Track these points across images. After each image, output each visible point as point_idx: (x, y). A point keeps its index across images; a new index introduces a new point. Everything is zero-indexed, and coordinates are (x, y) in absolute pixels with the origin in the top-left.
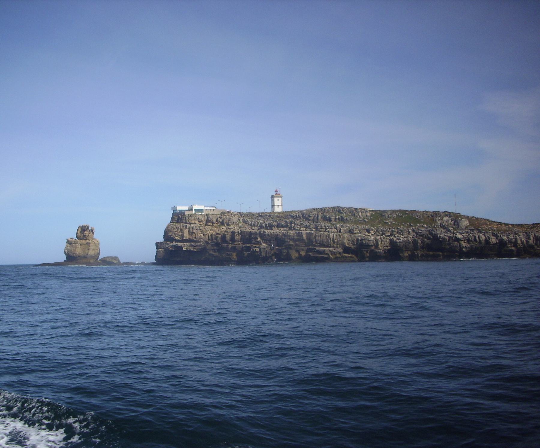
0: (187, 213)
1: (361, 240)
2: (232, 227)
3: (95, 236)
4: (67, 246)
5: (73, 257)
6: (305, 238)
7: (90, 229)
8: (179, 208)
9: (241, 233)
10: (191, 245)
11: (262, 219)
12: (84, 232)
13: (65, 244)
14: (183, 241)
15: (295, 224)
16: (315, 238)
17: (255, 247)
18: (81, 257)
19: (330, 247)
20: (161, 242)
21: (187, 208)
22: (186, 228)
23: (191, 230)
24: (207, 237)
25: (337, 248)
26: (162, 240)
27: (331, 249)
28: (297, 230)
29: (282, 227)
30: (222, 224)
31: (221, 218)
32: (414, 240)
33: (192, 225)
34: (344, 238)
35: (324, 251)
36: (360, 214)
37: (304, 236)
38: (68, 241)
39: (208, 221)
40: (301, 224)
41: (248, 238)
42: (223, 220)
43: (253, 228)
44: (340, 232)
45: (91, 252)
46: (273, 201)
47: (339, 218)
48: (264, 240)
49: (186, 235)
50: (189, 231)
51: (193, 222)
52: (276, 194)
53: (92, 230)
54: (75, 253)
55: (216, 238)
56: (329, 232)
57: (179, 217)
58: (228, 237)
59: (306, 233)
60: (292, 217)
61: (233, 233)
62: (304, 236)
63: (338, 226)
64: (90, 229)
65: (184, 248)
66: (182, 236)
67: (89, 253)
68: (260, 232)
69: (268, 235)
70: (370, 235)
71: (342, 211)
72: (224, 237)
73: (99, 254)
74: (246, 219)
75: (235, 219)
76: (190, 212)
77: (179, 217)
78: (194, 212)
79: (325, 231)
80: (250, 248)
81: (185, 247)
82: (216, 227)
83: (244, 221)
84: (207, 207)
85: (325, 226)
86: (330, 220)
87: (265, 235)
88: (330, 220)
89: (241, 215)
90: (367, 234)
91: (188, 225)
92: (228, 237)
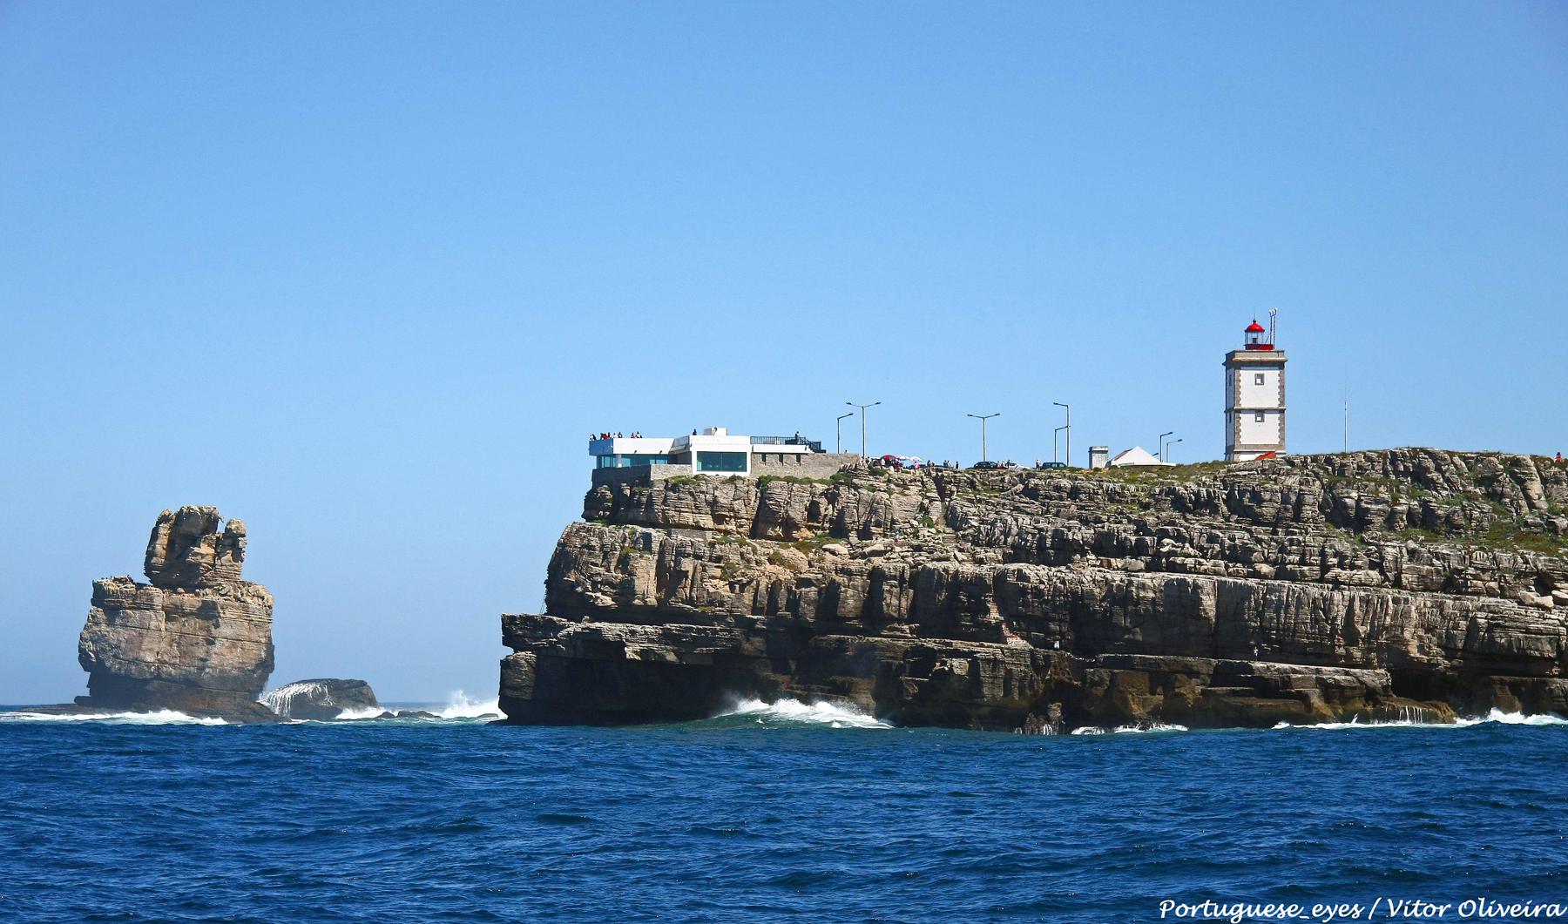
0: (660, 473)
1: (1490, 628)
2: (878, 544)
3: (247, 570)
4: (93, 620)
5: (127, 677)
6: (1212, 614)
7: (221, 528)
8: (622, 446)
9: (920, 580)
10: (667, 637)
11: (1035, 506)
12: (189, 549)
13: (84, 606)
14: (626, 609)
16: (1260, 615)
17: (957, 654)
18: (171, 680)
19: (1332, 660)
20: (527, 619)
21: (665, 446)
22: (647, 547)
23: (670, 559)
24: (748, 597)
25: (1367, 665)
26: (536, 605)
27: (1328, 672)
28: (1183, 568)
29: (1122, 550)
30: (838, 530)
31: (832, 498)
33: (679, 537)
34: (1406, 615)
35: (1286, 681)
36: (1536, 488)
37: (1209, 602)
38: (100, 595)
39: (767, 520)
40: (1212, 539)
41: (946, 605)
42: (841, 513)
43: (982, 553)
44: (1397, 583)
45: (225, 657)
47: (1410, 513)
48: (1020, 617)
49: (646, 583)
50: (661, 568)
51: (689, 518)
53: (231, 543)
54: (137, 661)
55: (793, 604)
56: (1337, 584)
57: (620, 491)
58: (851, 600)
59: (1221, 589)
60: (1179, 503)
61: (877, 576)
62: (1209, 602)
63: (1390, 552)
64: (221, 528)
65: (630, 652)
66: (625, 590)
67: (214, 661)
68: (1000, 578)
69: (1038, 593)
70: (1548, 601)
71: (1435, 475)
72: (830, 594)
74: (959, 502)
75: (902, 506)
76: (676, 470)
77: (620, 491)
78: (694, 468)
79: (1322, 580)
80: (931, 655)
81: (636, 640)
82: (803, 546)
84: (772, 441)
85: (1323, 554)
86: (1357, 522)
87: (1023, 591)
88: (1357, 522)
89: (941, 480)
90: (1533, 596)
91: (657, 535)
92: (851, 600)
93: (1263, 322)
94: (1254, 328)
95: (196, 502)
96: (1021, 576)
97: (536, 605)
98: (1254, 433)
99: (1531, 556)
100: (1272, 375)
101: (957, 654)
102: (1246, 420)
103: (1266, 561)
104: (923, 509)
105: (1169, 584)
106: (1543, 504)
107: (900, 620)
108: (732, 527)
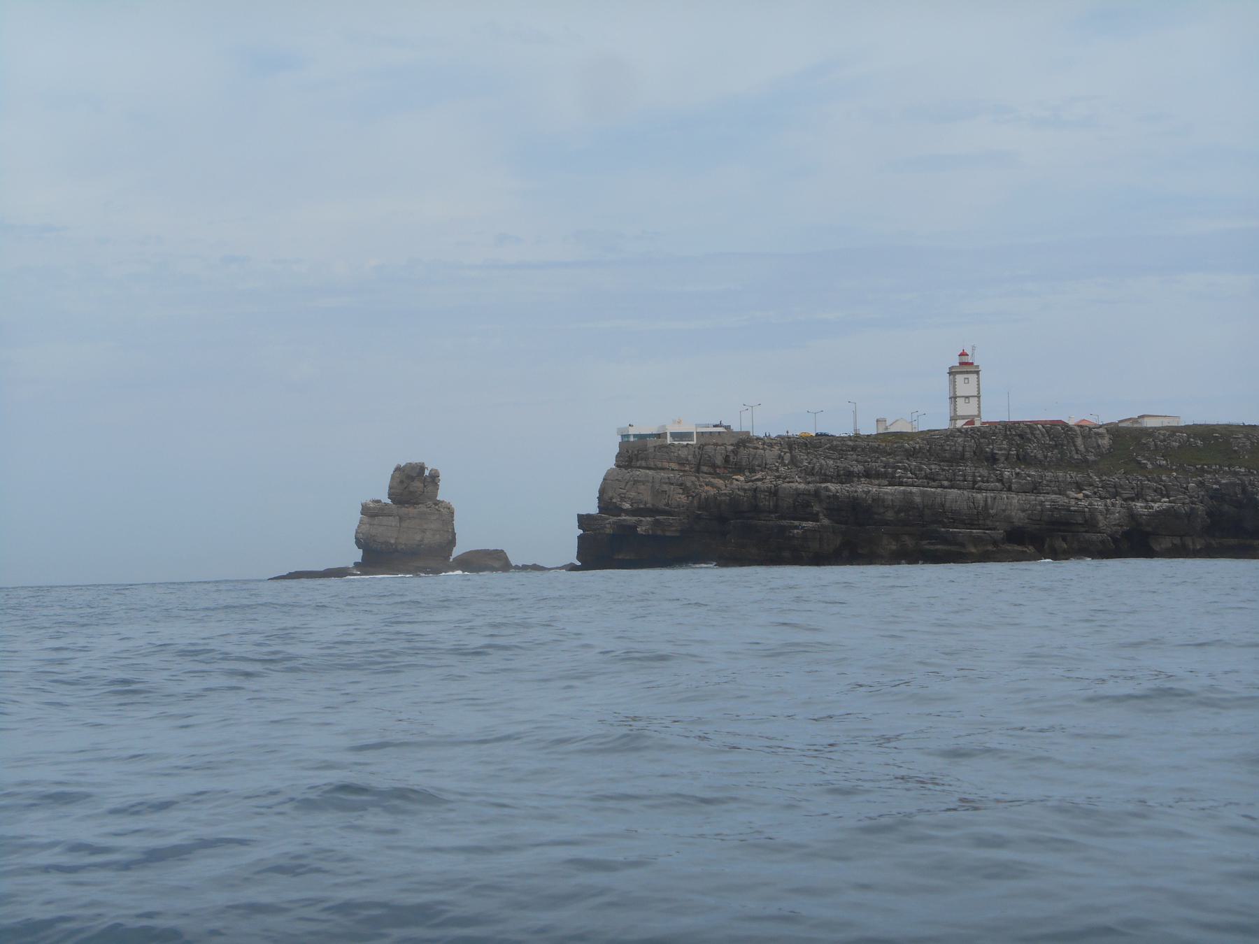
7: (427, 473)
12: (414, 486)
13: (357, 516)
15: (905, 469)
17: (796, 527)
20: (588, 516)
26: (593, 509)
29: (878, 475)
30: (740, 470)
32: (1192, 509)
36: (1079, 441)
38: (366, 510)
46: (953, 384)
52: (962, 364)
67: (426, 541)
70: (1080, 496)
73: (452, 542)
81: (644, 526)
83: (794, 461)
85: (974, 476)
86: (993, 459)
93: (968, 351)
94: (963, 354)
95: (416, 459)
96: (827, 489)
97: (593, 509)
98: (965, 409)
99: (1074, 474)
100: (973, 377)
101: (796, 527)
102: (960, 401)
103: (947, 479)
104: (780, 457)
105: (904, 492)
106: (1082, 448)
107: (770, 512)
108: (687, 468)
